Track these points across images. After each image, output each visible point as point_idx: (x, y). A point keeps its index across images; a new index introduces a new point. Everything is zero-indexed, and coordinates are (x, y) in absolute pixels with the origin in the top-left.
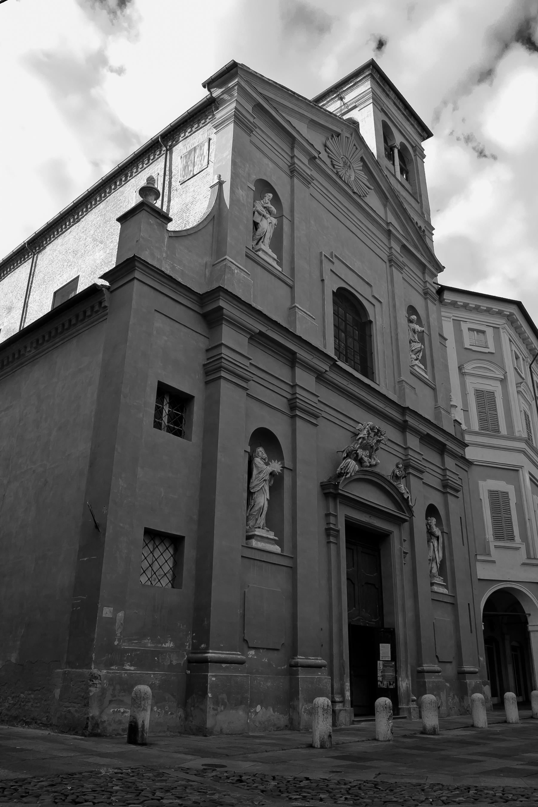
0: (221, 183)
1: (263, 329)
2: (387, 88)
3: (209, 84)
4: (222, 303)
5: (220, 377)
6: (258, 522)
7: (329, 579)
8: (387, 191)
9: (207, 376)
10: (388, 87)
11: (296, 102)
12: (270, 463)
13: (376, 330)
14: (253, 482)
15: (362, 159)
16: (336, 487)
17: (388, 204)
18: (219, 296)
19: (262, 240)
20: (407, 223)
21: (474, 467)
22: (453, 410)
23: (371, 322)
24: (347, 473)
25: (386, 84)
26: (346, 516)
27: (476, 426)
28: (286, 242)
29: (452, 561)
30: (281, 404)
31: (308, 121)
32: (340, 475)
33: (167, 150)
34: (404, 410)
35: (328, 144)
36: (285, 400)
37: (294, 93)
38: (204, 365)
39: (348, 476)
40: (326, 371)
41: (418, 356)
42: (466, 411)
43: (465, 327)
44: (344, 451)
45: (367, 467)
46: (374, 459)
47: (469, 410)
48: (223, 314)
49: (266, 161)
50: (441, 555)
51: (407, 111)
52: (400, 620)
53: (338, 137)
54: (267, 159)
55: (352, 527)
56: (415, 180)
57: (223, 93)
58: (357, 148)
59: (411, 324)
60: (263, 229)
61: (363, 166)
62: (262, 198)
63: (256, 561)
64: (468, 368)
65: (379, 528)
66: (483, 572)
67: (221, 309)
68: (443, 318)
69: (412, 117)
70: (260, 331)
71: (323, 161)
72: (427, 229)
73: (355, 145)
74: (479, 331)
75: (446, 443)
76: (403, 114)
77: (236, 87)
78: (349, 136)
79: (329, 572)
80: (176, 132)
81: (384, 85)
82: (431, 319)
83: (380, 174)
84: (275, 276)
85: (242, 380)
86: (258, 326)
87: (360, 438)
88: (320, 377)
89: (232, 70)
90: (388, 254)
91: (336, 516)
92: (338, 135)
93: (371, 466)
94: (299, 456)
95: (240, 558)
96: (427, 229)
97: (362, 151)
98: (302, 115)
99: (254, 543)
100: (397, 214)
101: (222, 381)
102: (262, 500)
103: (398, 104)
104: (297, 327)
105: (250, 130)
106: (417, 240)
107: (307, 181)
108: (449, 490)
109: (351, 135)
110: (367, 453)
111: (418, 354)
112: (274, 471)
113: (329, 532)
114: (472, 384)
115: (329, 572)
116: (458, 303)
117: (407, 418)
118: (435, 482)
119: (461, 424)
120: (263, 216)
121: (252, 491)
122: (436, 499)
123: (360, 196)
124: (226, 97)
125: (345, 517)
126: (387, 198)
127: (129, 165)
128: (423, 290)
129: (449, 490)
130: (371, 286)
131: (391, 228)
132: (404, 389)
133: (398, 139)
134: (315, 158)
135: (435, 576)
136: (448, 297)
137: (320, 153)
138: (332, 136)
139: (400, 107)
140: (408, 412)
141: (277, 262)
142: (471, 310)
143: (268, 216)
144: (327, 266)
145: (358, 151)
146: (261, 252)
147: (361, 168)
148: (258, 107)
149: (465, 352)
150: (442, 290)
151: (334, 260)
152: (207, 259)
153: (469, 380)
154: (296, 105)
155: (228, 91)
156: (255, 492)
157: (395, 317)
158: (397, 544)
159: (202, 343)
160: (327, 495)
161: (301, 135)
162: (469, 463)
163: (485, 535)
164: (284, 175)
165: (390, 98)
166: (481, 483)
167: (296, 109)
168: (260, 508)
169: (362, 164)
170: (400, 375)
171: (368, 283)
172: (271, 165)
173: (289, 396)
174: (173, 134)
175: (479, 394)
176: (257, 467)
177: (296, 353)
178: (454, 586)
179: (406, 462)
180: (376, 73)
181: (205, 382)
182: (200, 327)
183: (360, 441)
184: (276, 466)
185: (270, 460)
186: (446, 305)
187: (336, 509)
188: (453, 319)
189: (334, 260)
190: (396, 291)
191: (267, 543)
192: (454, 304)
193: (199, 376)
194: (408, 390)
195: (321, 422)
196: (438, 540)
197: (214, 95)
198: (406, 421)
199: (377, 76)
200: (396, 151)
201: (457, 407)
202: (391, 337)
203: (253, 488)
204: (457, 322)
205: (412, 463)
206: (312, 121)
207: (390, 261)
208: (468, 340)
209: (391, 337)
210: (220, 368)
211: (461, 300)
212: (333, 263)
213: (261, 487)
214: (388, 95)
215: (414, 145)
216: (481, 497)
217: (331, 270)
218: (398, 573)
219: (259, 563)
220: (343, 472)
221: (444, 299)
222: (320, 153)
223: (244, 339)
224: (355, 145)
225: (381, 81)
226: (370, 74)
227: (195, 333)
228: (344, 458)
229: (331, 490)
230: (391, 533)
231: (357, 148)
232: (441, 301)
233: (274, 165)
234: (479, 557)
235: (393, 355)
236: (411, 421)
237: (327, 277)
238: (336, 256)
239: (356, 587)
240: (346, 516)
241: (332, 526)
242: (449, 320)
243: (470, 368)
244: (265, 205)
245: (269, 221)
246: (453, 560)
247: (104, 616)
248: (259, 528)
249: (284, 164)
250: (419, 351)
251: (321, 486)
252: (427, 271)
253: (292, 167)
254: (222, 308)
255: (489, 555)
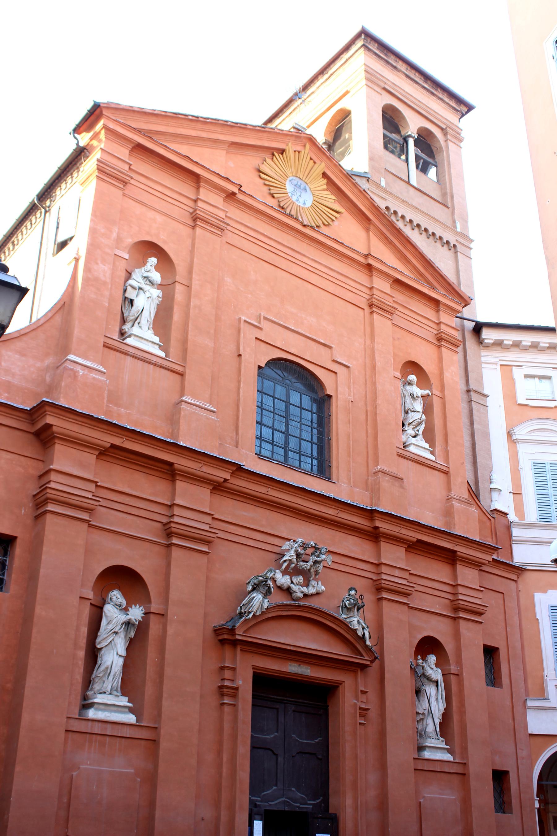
0: (77, 260)
1: (117, 441)
2: (392, 60)
3: (77, 130)
4: (49, 420)
5: (46, 512)
6: (104, 685)
7: (219, 753)
8: (368, 209)
9: (38, 509)
10: (393, 57)
11: (203, 127)
12: (130, 609)
13: (337, 406)
14: (100, 636)
15: (325, 175)
16: (232, 631)
17: (371, 227)
18: (46, 411)
19: (138, 321)
20: (405, 247)
21: (528, 575)
22: (495, 495)
23: (330, 397)
24: (249, 613)
25: (389, 54)
26: (254, 667)
27: (532, 514)
28: (177, 316)
29: (462, 713)
30: (148, 530)
31: (226, 146)
32: (241, 615)
33: (46, 212)
34: (371, 514)
35: (265, 168)
36: (159, 525)
37: (197, 117)
38: (34, 496)
39: (251, 615)
40: (226, 480)
41: (418, 431)
42: (517, 494)
43: (518, 374)
44: (249, 583)
45: (298, 599)
46: (314, 587)
47: (523, 494)
48: (53, 433)
49: (151, 214)
50: (442, 706)
51: (429, 82)
52: (349, 801)
53: (282, 154)
54: (153, 212)
55: (263, 682)
56: (444, 176)
57: (92, 139)
58: (315, 163)
59: (408, 388)
60: (138, 307)
61: (327, 184)
62: (144, 263)
63: (94, 736)
64: (520, 432)
65: (316, 678)
66: (537, 723)
67: (49, 426)
68: (483, 365)
69: (439, 90)
70: (112, 444)
71: (249, 195)
72: (460, 243)
73: (311, 159)
74: (541, 377)
75: (456, 548)
76: (424, 87)
77: (103, 132)
78: (299, 148)
79: (220, 743)
80: (53, 189)
81: (386, 55)
82: (447, 375)
83: (355, 190)
84: (155, 365)
85: (83, 511)
86: (108, 439)
87: (285, 561)
88: (218, 488)
89: (95, 113)
90: (368, 297)
91: (234, 669)
92: (282, 152)
93: (306, 596)
94: (174, 595)
95: (62, 734)
96: (460, 243)
97: (323, 165)
98: (216, 141)
99: (92, 714)
100: (386, 238)
101: (49, 516)
102: (113, 657)
103: (412, 76)
104: (181, 428)
105: (124, 182)
106: (424, 267)
107: (219, 227)
108: (461, 615)
109: (305, 146)
110: (300, 579)
111: (418, 428)
112: (130, 619)
113: (224, 691)
114: (527, 455)
115: (220, 743)
116: (505, 342)
117: (378, 524)
118: (437, 605)
119: (507, 514)
120: (140, 288)
121: (98, 646)
122: (439, 629)
123: (312, 227)
124: (95, 143)
125: (253, 668)
126: (369, 220)
127: (14, 230)
128: (436, 335)
129: (461, 615)
130: (330, 347)
131: (371, 261)
132: (379, 483)
133: (413, 124)
134: (234, 194)
135: (430, 737)
136: (488, 335)
137: (241, 186)
138: (273, 155)
139: (416, 79)
140: (376, 515)
141: (160, 347)
142: (525, 349)
143: (146, 287)
144: (249, 334)
145: (316, 165)
146: (133, 337)
147: (325, 187)
148: (139, 148)
149: (518, 411)
150: (478, 328)
151: (264, 324)
152: (49, 361)
153: (522, 449)
154: (204, 130)
155: (96, 136)
156: (102, 648)
157: (374, 384)
158: (351, 696)
159: (34, 469)
160: (223, 642)
161: (209, 169)
162: (519, 570)
163: (543, 671)
164: (181, 227)
165: (399, 71)
166: (538, 596)
167: (204, 135)
168: (107, 668)
169: (325, 181)
170: (377, 463)
171: (324, 345)
172: (159, 218)
173: (165, 520)
174: (50, 192)
175: (538, 467)
176: (106, 616)
177: (173, 463)
178: (464, 749)
179: (377, 583)
180: (372, 42)
181: (35, 517)
182: (30, 448)
183: (285, 565)
184: (136, 613)
185: (129, 604)
186: (487, 346)
187: (234, 660)
188: (501, 365)
189: (264, 324)
190: (376, 347)
191: (112, 711)
192: (499, 344)
193: (26, 511)
194: (385, 483)
195: (221, 550)
196: (437, 686)
197: (82, 144)
198: (377, 528)
199: (374, 47)
200: (411, 142)
201: (501, 491)
202: (367, 412)
203: (100, 643)
204: (507, 369)
205: (384, 584)
206: (234, 144)
207: (371, 305)
208: (526, 390)
209: (367, 412)
210: (46, 501)
211: (508, 337)
212: (261, 329)
213: (109, 641)
214: (395, 68)
215: (444, 127)
216: (538, 616)
217: (256, 338)
218: (348, 737)
219: (99, 737)
220: (243, 611)
221: (483, 340)
222: (241, 186)
223: (90, 458)
224: (311, 159)
225: (383, 52)
226: (363, 45)
227: (23, 459)
228: (250, 592)
229: (226, 636)
230: (341, 684)
231: (315, 163)
232: (480, 342)
233: (164, 218)
234: (530, 703)
235: (367, 437)
236: (383, 526)
237: (248, 350)
238: (265, 318)
239: (280, 759)
240: (254, 667)
241: (227, 683)
242: (494, 366)
243: (524, 432)
244: (146, 274)
245: (148, 294)
246: (465, 712)
247: (255, 821)
248: (105, 693)
249: (181, 212)
250: (420, 424)
251: (215, 631)
252: (441, 308)
253: (194, 214)
254: (51, 426)
255: (546, 699)
